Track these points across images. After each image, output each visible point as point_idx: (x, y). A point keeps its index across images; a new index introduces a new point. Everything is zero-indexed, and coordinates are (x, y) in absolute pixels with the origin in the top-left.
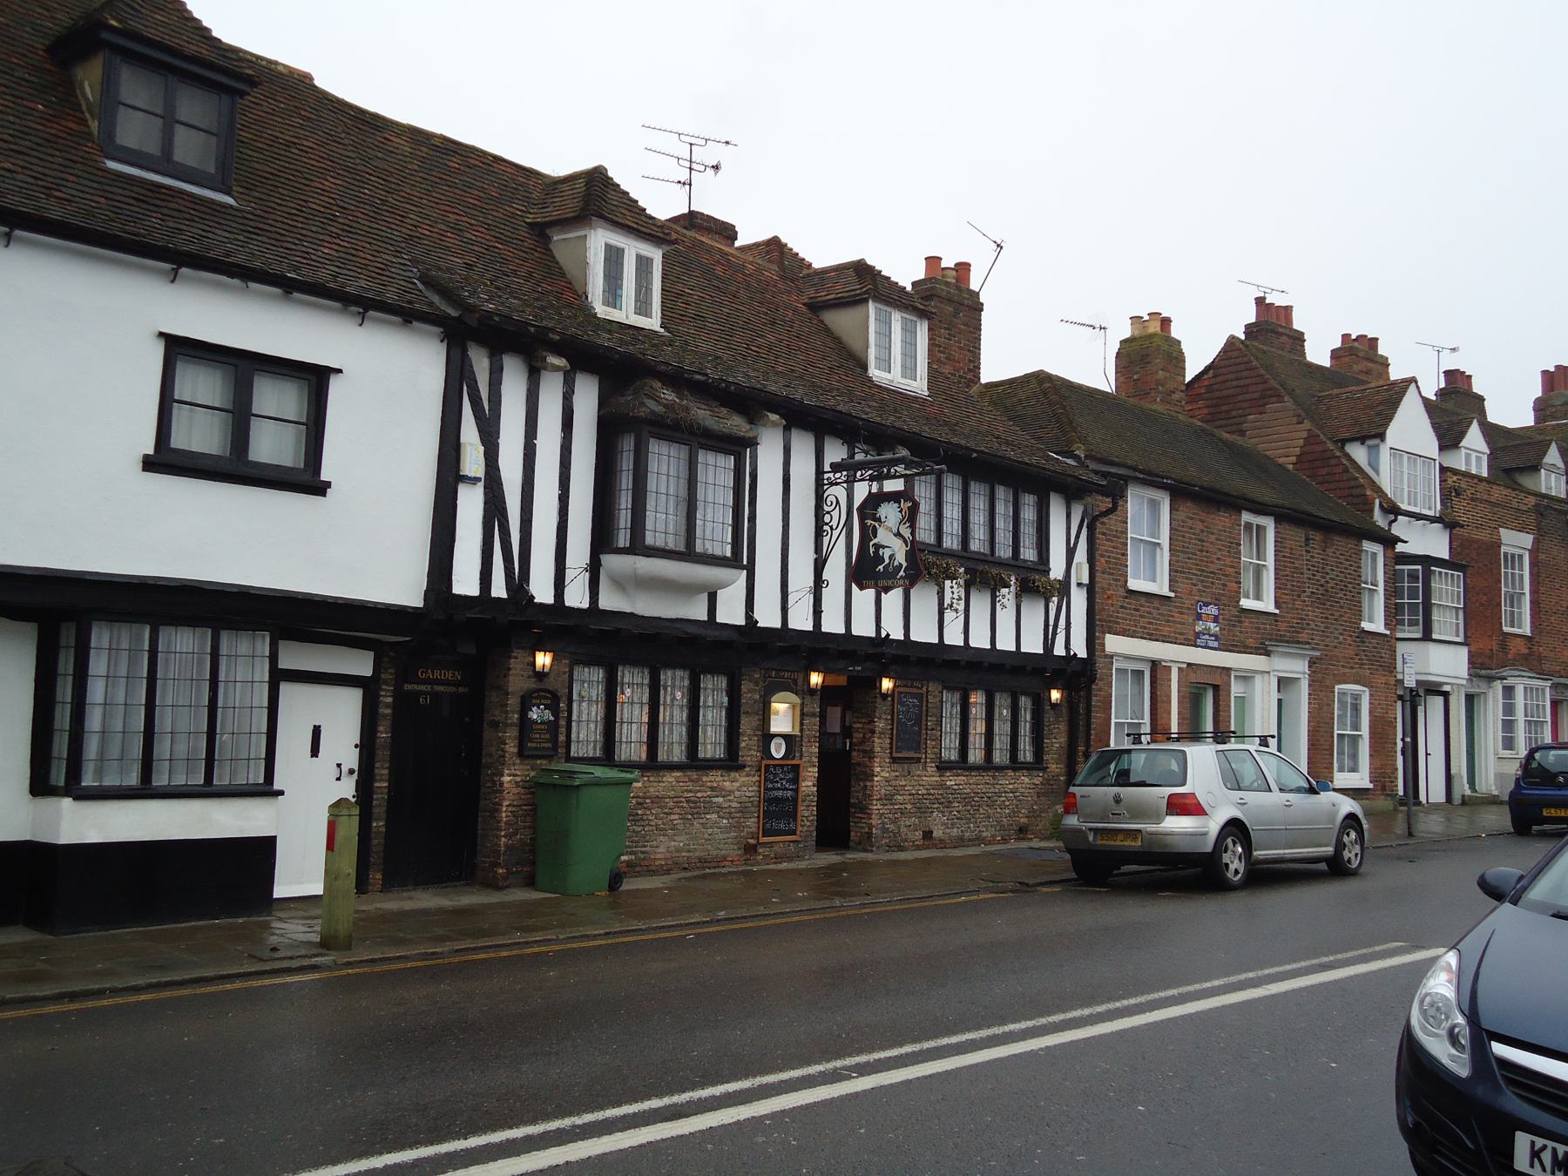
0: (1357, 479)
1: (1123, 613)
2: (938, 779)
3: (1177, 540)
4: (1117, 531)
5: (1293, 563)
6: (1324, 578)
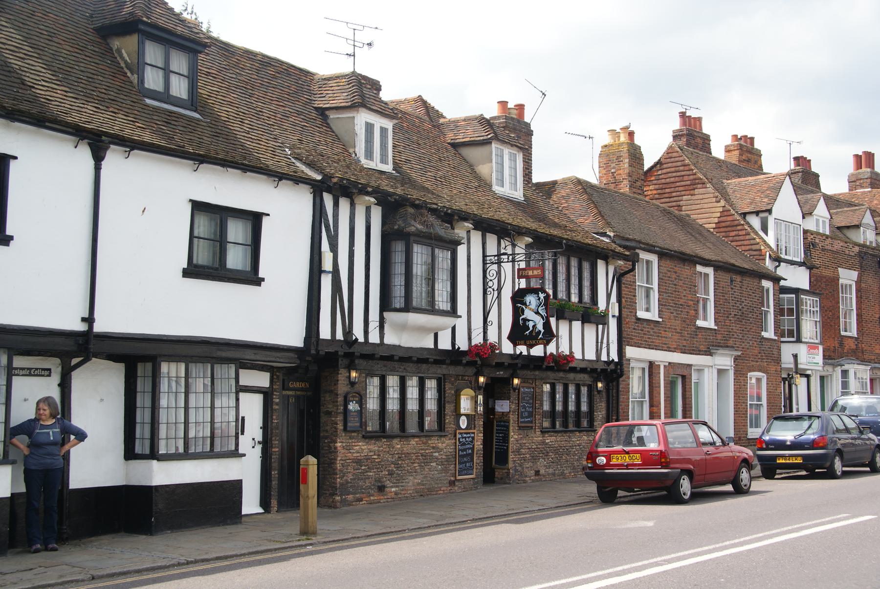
0: (754, 239)
1: (635, 333)
2: (541, 438)
3: (662, 285)
4: (630, 281)
5: (724, 296)
6: (741, 305)
